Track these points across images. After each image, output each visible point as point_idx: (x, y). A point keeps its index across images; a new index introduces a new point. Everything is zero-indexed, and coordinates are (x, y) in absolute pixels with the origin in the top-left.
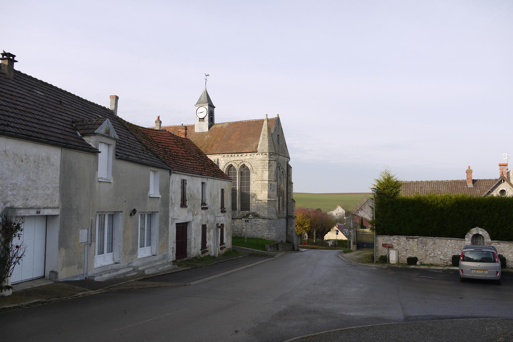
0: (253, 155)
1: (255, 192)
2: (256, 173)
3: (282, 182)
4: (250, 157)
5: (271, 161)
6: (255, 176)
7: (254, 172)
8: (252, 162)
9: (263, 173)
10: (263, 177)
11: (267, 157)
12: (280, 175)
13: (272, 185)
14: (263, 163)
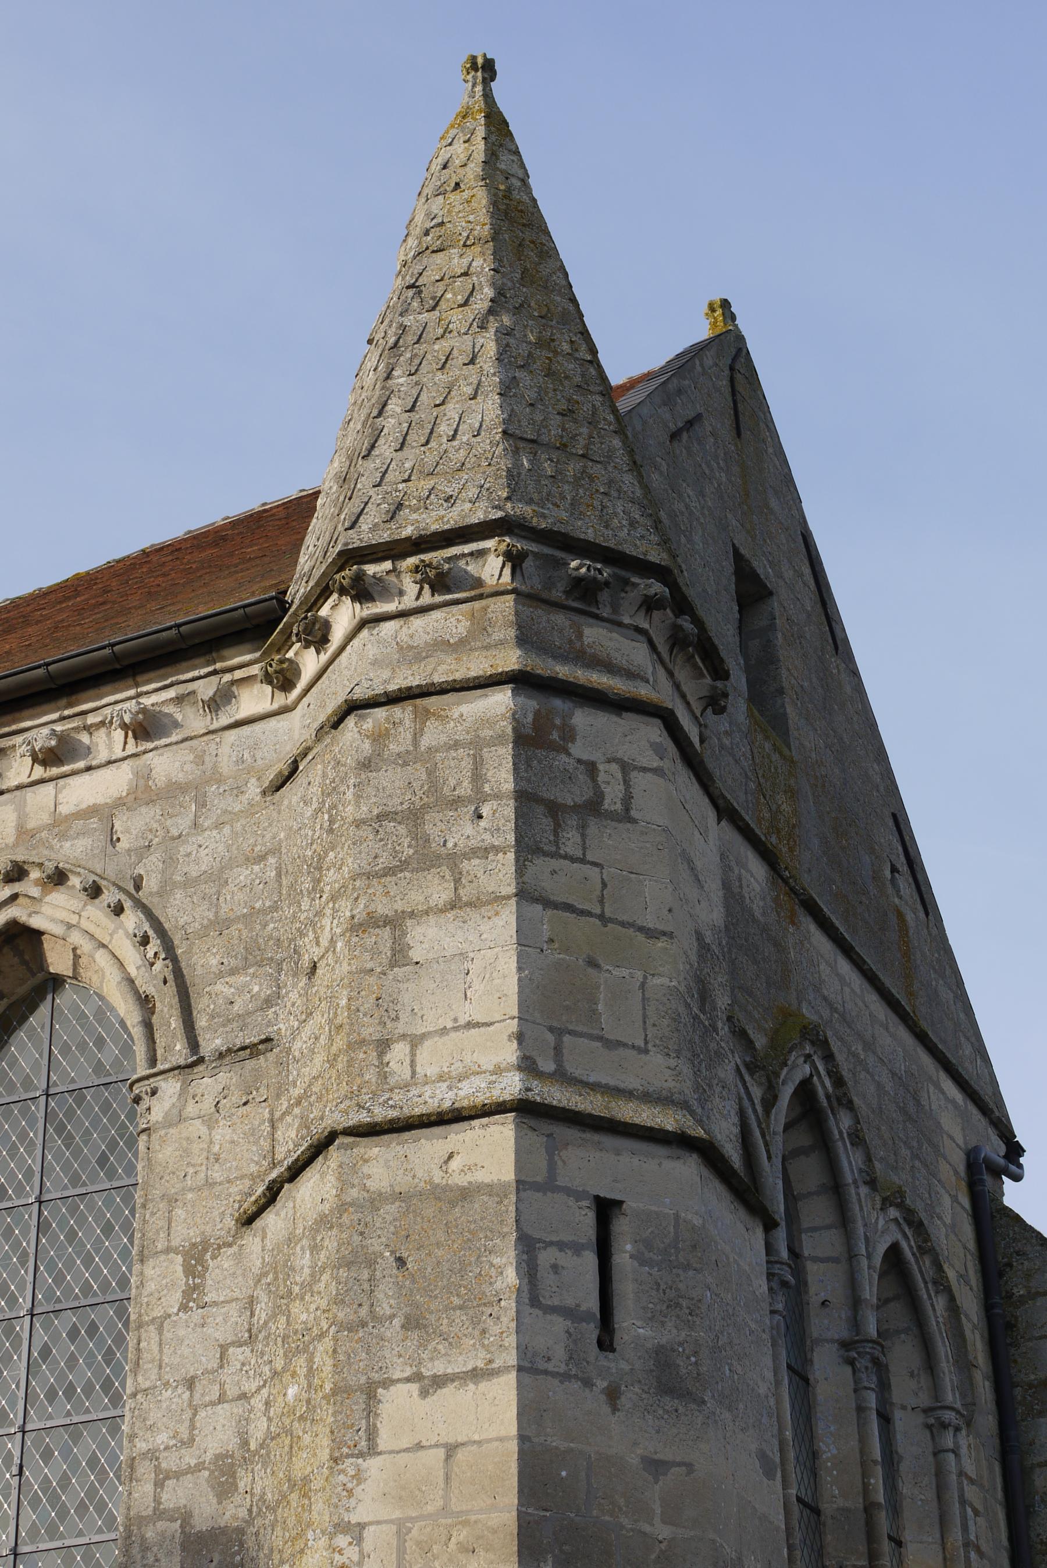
0: (194, 721)
1: (225, 1488)
2: (253, 1050)
3: (906, 1488)
4: (144, 776)
5: (583, 719)
6: (222, 1133)
7: (211, 1043)
8: (170, 861)
9: (399, 955)
10: (399, 1051)
11: (480, 627)
12: (856, 1302)
13: (622, 1227)
14: (404, 760)
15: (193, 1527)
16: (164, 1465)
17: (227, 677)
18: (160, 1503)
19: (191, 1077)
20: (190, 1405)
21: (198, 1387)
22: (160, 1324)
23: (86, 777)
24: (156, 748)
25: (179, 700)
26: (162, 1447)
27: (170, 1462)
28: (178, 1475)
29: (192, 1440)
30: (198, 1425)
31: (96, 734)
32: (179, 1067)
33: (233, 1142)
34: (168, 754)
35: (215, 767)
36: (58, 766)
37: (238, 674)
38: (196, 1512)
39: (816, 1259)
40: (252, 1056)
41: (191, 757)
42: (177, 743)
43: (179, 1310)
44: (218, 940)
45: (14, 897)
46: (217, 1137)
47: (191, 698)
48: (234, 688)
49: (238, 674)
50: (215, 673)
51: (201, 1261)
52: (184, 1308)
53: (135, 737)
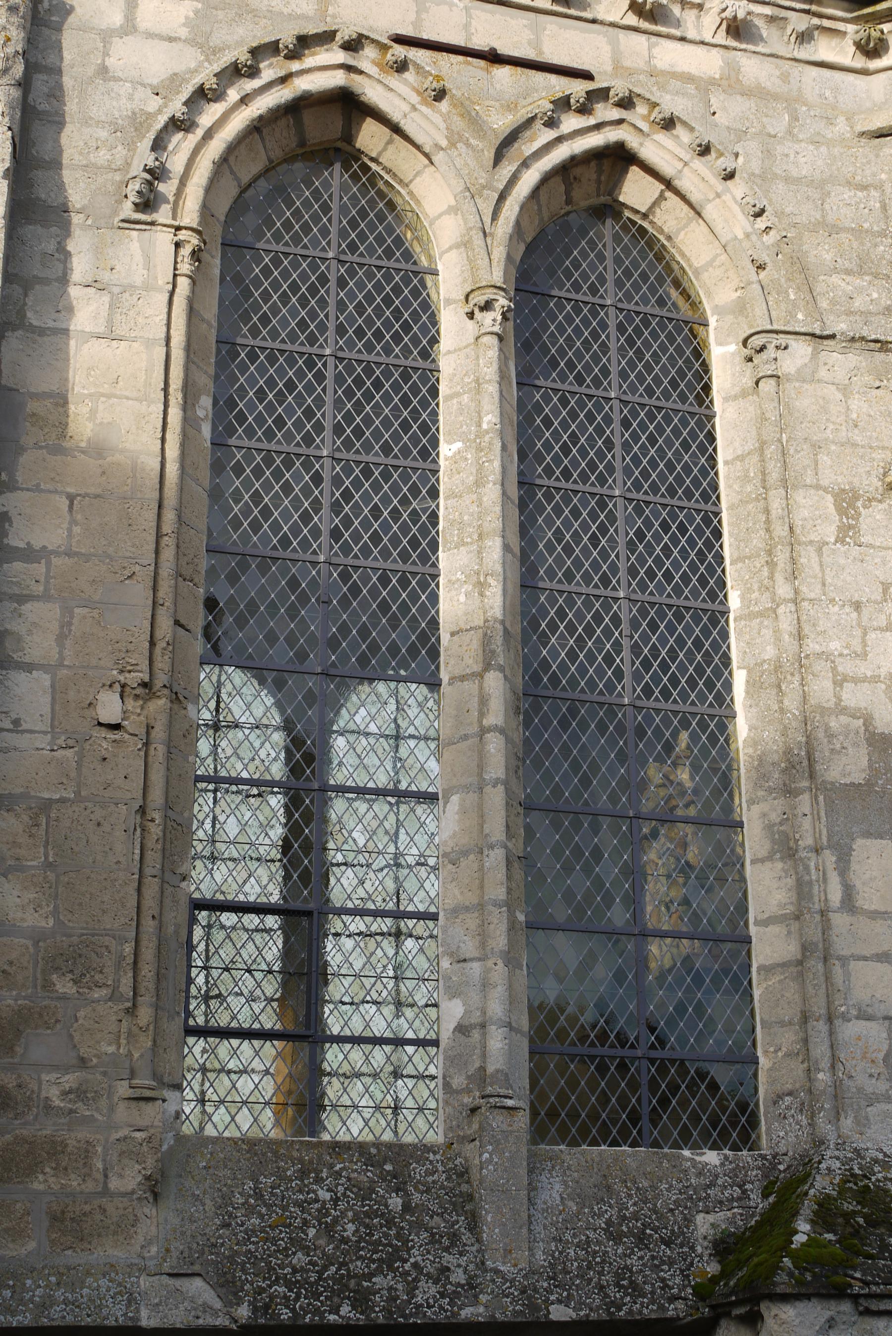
15: (875, 728)
16: (840, 669)
17: (816, 21)
18: (841, 700)
19: (822, 347)
20: (859, 625)
21: (866, 612)
22: (820, 548)
23: (678, 45)
24: (745, 50)
25: (772, 19)
26: (836, 653)
27: (846, 667)
28: (856, 680)
29: (866, 654)
30: (869, 643)
31: (687, 11)
32: (813, 335)
33: (870, 416)
34: (755, 60)
35: (800, 90)
36: (650, 23)
37: (826, 23)
38: (876, 716)
39: (237, 179)
40: (880, 350)
41: (778, 73)
42: (764, 55)
43: (836, 541)
44: (828, 240)
45: (620, 122)
46: (853, 407)
47: (782, 23)
48: (816, 33)
49: (826, 23)
50: (807, 12)
51: (852, 505)
52: (840, 540)
53: (728, 32)
